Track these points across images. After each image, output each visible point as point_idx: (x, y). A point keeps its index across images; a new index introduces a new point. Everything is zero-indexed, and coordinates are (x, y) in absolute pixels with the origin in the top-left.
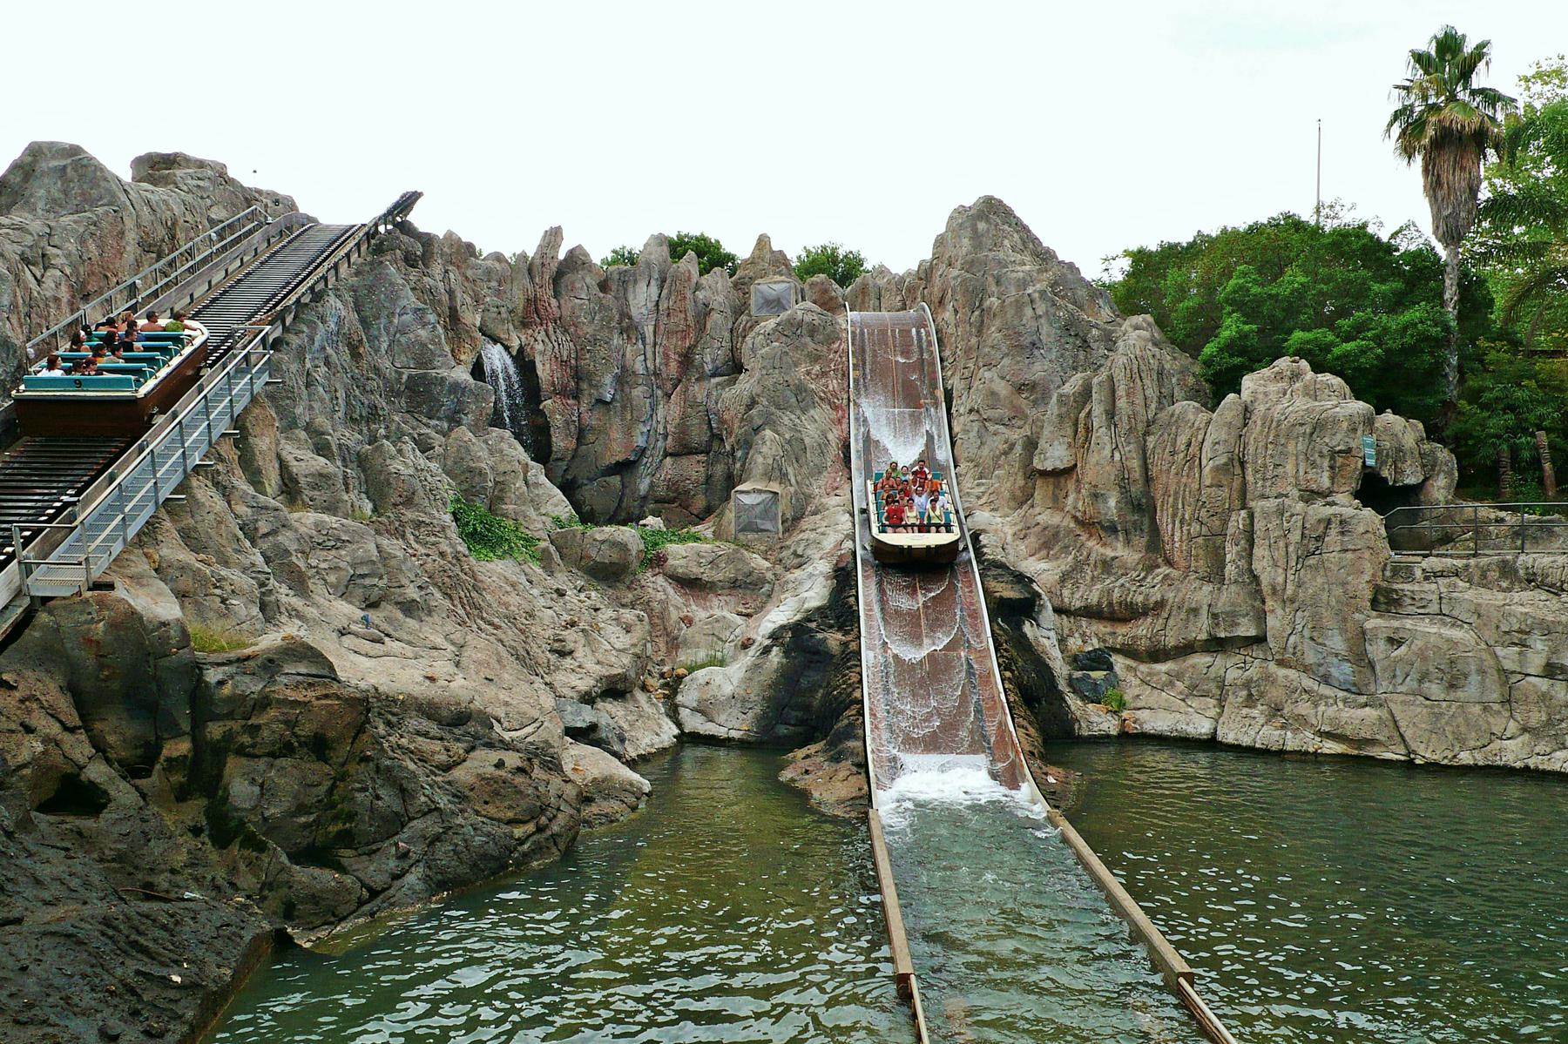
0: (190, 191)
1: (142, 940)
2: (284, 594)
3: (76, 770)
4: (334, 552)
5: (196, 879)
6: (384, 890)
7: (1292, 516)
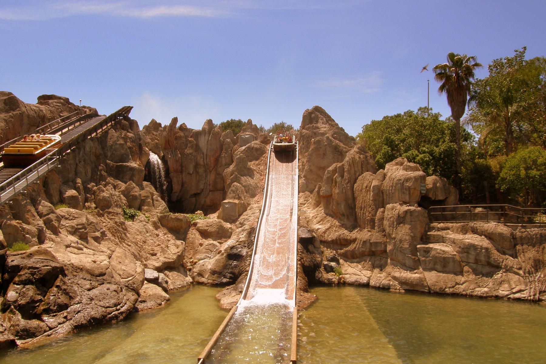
0: (53, 107)
2: (48, 234)
4: (72, 221)
6: (55, 328)
7: (396, 210)
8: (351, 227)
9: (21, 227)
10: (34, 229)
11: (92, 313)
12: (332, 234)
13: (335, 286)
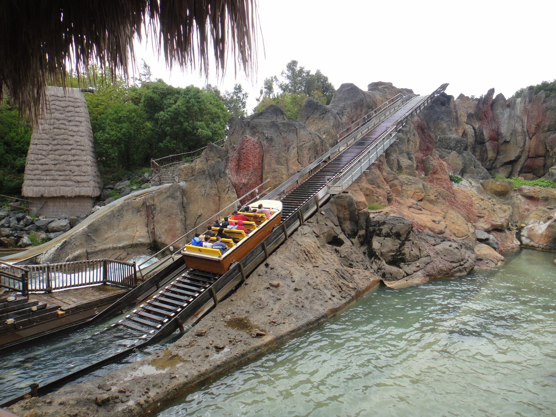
1: (344, 276)
3: (337, 235)
5: (362, 265)
6: (411, 274)
10: (384, 193)
11: (441, 265)
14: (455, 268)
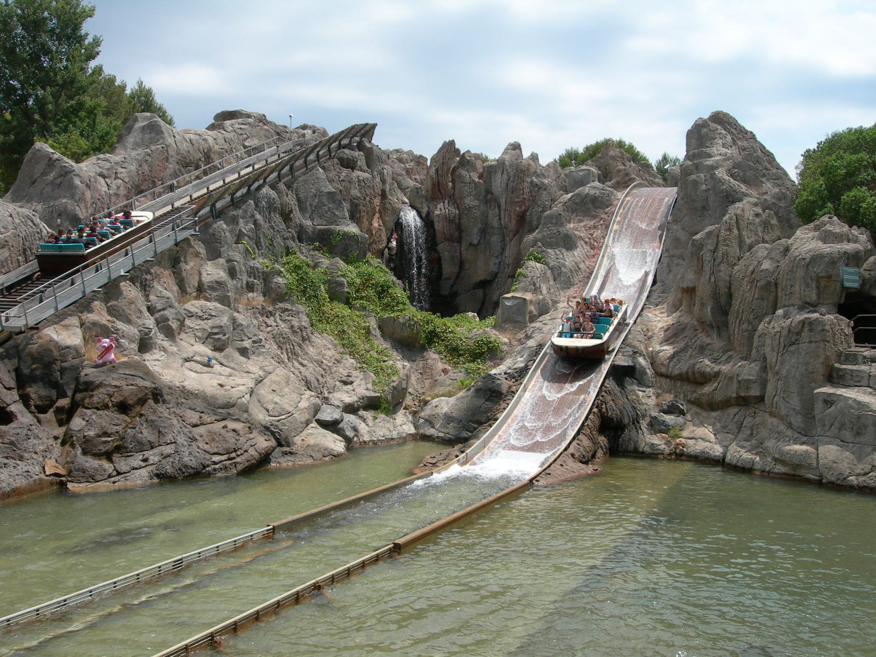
3: (5, 405)
4: (205, 321)
6: (125, 473)
8: (720, 351)
9: (113, 327)
10: (132, 331)
12: (683, 362)
13: (663, 460)
14: (218, 464)
